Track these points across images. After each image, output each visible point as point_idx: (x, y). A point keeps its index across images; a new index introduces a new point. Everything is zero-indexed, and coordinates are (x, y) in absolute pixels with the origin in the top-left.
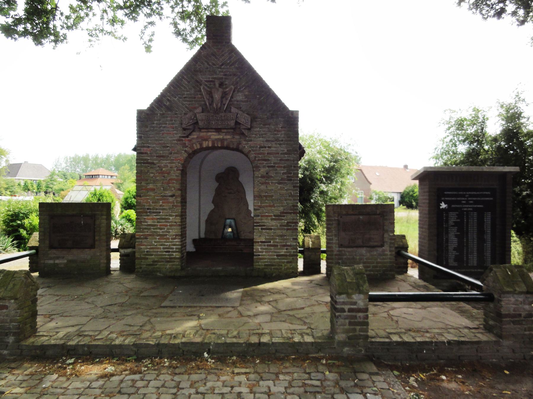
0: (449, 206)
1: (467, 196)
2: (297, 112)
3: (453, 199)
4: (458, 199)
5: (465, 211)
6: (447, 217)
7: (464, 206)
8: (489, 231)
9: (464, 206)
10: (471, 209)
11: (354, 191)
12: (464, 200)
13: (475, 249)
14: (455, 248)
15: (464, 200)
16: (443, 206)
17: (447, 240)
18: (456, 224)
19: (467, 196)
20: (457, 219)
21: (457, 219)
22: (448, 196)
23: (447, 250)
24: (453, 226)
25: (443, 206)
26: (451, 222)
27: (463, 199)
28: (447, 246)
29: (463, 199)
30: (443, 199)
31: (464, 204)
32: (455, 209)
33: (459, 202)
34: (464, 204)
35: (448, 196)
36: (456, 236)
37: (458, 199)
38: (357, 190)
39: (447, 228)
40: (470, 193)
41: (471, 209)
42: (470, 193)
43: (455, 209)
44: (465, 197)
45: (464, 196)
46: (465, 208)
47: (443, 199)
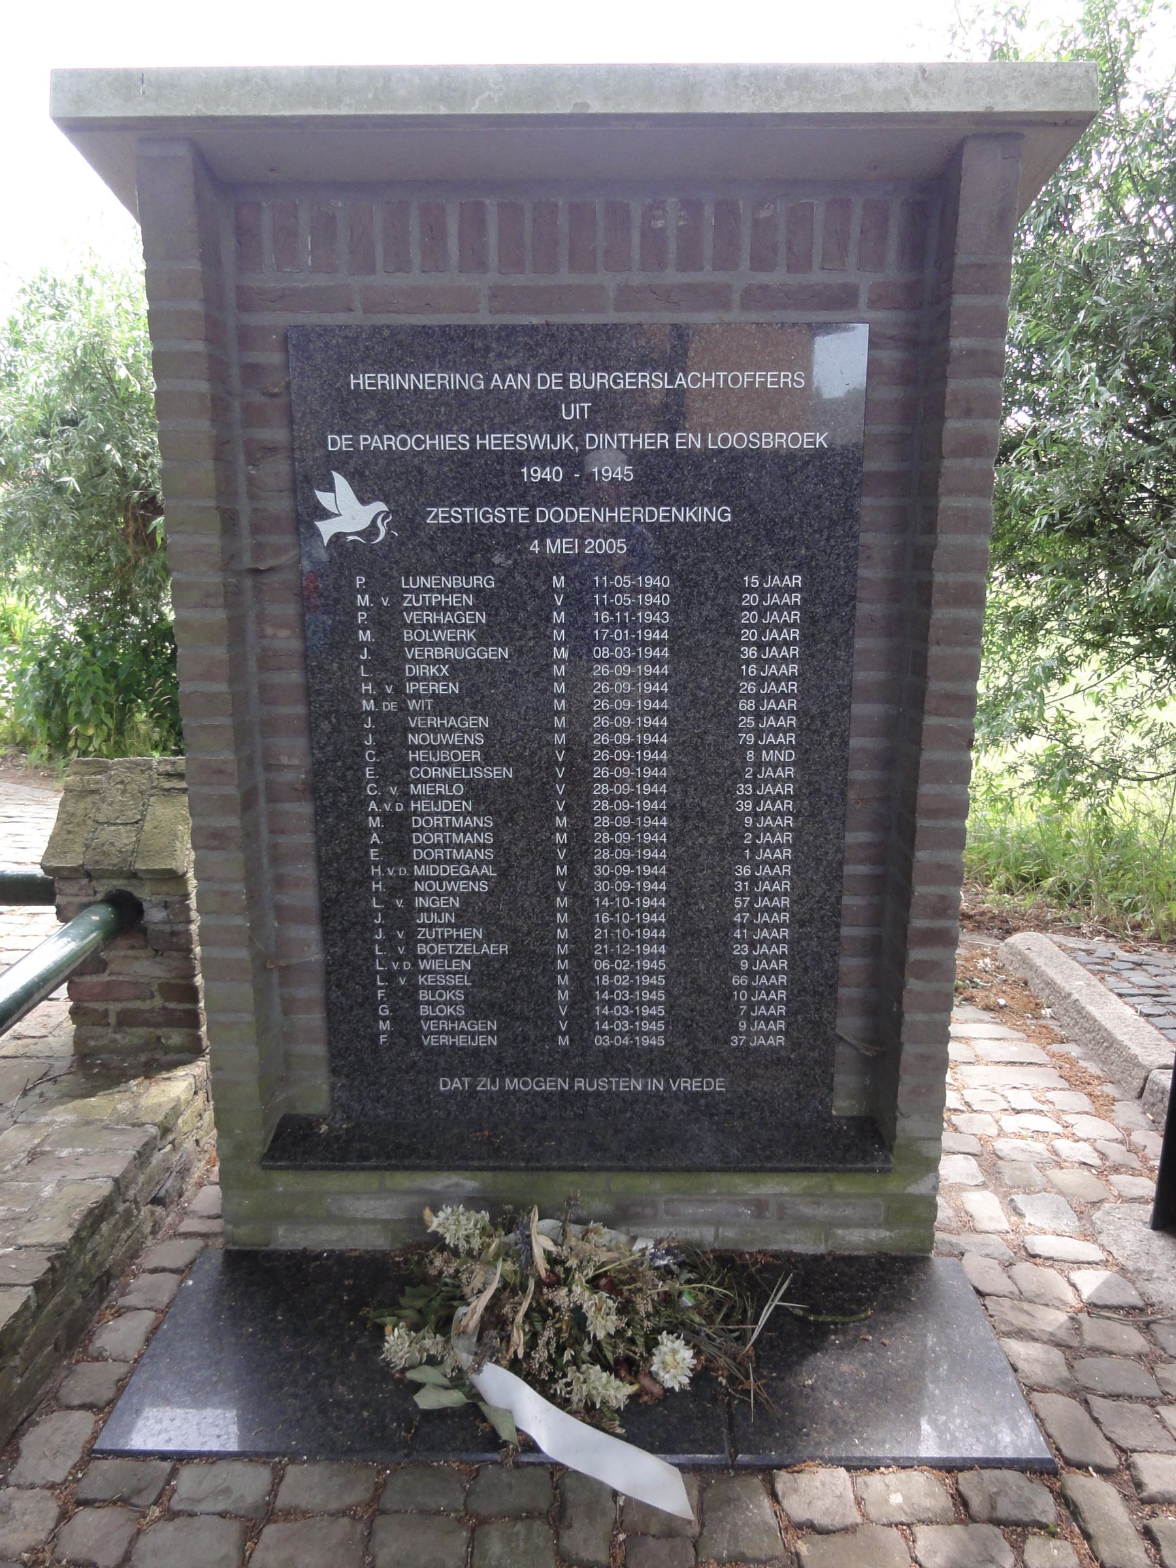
0: (406, 521)
1: (572, 412)
2: (220, 183)
3: (443, 443)
4: (490, 442)
5: (562, 563)
6: (387, 622)
7: (547, 515)
8: (781, 754)
9: (547, 515)
10: (619, 546)
11: (1113, 145)
12: (543, 458)
13: (654, 904)
14: (467, 899)
15: (543, 458)
16: (347, 512)
17: (399, 827)
18: (473, 688)
19: (572, 412)
20: (484, 637)
21: (484, 637)
22: (392, 411)
23: (404, 921)
24: (443, 705)
25: (347, 512)
26: (427, 675)
27: (539, 441)
28: (404, 887)
29: (539, 441)
30: (340, 442)
31: (549, 494)
32: (466, 549)
33: (494, 478)
34: (549, 494)
35: (392, 411)
36: (479, 794)
37: (490, 442)
38: (1111, 154)
39: (393, 729)
40: (600, 380)
41: (619, 546)
42: (600, 380)
43: (466, 549)
44: (558, 427)
45: (544, 411)
46: (563, 530)
47: (340, 442)
